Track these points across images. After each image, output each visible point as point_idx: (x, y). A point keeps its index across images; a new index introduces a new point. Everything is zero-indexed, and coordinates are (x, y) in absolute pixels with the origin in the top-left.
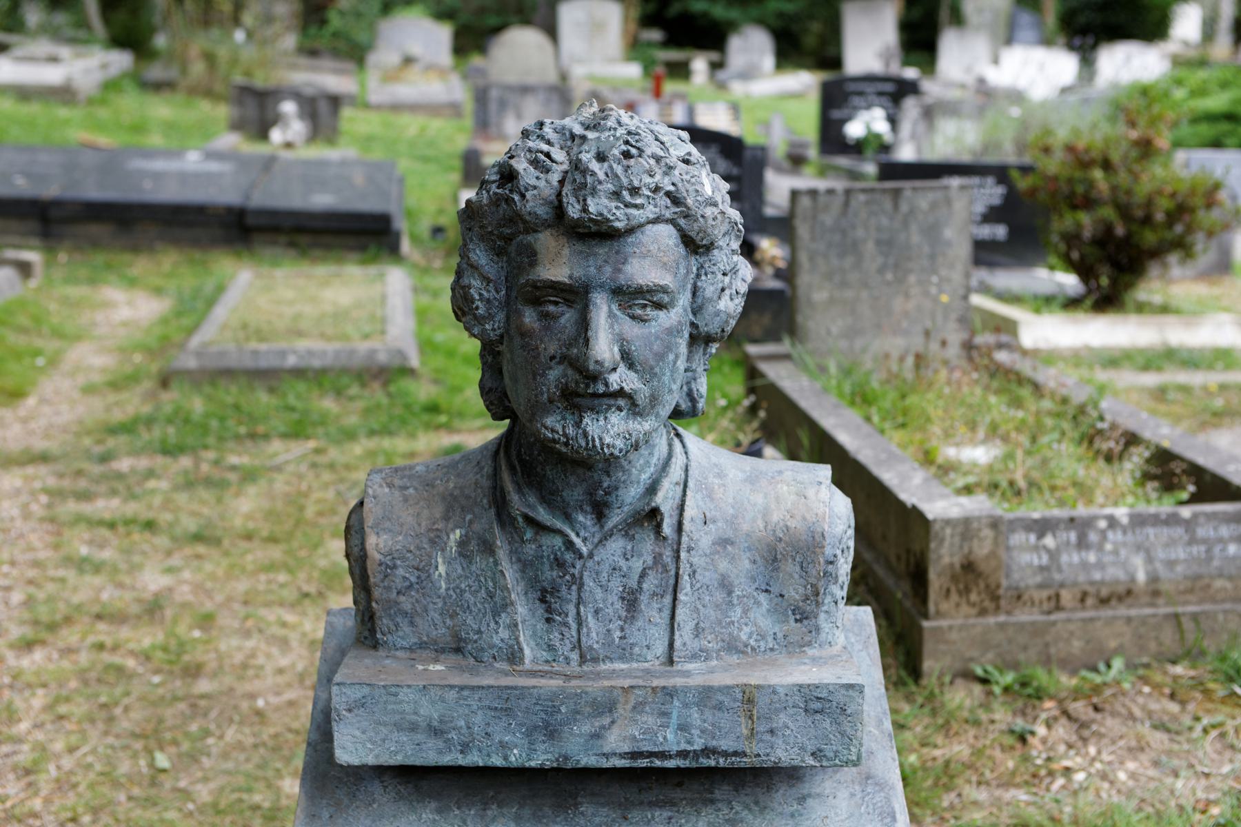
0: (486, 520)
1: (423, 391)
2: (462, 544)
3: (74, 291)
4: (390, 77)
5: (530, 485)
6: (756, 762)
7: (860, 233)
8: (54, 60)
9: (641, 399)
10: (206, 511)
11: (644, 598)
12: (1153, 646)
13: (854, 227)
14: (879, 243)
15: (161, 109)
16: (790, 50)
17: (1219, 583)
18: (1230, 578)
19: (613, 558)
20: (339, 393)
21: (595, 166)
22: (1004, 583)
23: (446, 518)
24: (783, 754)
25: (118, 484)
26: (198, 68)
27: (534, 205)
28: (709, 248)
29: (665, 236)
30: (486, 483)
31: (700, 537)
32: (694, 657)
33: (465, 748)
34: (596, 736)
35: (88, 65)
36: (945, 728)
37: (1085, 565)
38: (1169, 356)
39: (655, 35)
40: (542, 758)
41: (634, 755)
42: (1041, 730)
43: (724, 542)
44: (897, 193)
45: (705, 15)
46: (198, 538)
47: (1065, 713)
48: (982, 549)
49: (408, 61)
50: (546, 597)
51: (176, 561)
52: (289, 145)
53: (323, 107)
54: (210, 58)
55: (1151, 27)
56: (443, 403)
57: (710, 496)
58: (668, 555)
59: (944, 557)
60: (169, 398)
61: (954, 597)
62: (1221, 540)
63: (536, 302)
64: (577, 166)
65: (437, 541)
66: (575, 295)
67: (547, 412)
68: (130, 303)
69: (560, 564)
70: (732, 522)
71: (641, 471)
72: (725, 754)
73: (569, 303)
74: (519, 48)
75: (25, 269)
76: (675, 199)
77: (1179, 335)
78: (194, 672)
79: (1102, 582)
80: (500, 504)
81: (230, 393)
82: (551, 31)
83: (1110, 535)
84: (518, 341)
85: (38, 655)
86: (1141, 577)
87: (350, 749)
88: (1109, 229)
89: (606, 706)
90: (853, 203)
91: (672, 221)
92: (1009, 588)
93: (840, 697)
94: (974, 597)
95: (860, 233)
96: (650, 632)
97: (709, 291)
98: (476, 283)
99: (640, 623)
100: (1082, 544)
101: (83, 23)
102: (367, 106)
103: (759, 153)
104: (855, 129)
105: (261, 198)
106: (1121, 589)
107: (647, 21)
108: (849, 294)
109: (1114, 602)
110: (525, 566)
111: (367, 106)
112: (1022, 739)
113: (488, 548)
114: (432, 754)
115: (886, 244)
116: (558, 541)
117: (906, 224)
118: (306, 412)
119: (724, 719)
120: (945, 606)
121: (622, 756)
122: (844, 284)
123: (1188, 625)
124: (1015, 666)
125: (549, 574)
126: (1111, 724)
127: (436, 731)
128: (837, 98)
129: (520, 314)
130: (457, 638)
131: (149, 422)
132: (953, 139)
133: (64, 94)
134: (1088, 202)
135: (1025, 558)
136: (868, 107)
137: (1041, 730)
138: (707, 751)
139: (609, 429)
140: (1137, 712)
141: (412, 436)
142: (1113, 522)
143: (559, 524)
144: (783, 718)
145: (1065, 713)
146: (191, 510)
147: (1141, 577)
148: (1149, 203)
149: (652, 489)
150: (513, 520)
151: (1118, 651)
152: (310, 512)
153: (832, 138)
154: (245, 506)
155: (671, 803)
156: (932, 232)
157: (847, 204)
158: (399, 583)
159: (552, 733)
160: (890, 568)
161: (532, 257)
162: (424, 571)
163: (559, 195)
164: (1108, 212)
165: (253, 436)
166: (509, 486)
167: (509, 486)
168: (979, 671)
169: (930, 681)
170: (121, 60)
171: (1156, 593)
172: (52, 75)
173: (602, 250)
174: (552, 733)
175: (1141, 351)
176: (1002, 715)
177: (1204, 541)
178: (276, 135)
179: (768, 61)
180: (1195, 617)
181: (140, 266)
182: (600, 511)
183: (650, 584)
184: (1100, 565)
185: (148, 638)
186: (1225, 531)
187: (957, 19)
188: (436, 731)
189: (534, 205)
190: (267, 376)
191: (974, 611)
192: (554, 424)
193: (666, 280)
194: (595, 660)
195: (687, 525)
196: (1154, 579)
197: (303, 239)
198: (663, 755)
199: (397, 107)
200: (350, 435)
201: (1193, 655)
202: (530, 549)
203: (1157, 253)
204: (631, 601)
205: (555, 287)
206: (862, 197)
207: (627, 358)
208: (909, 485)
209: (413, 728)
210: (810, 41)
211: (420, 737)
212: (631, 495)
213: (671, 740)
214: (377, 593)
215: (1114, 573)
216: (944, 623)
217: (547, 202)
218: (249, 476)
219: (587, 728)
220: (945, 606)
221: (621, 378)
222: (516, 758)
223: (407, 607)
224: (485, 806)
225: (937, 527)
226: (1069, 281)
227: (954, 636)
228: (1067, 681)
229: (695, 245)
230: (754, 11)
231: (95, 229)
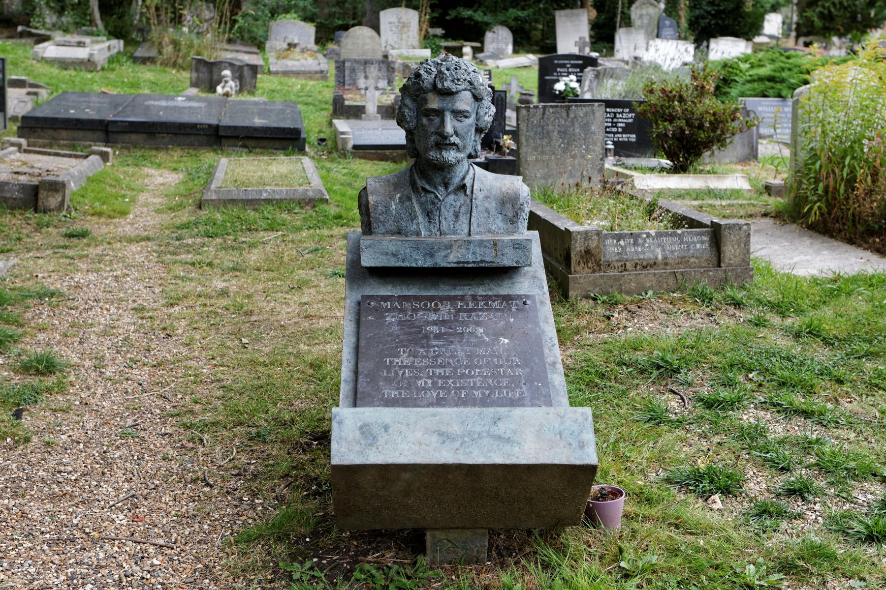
0: (408, 190)
1: (332, 210)
2: (400, 198)
3: (131, 170)
4: (282, 55)
5: (423, 178)
6: (498, 265)
7: (551, 127)
8: (80, 44)
9: (461, 146)
10: (235, 259)
11: (461, 215)
12: (665, 285)
13: (548, 124)
14: (559, 132)
15: (147, 74)
16: (522, 42)
17: (692, 260)
18: (697, 258)
19: (451, 202)
20: (289, 211)
21: (446, 72)
22: (603, 259)
23: (395, 190)
24: (507, 262)
25: (188, 249)
26: (169, 50)
27: (427, 84)
28: (482, 99)
29: (467, 95)
30: (408, 179)
31: (479, 195)
32: (477, 234)
33: (404, 260)
34: (446, 256)
35: (100, 48)
36: (578, 315)
37: (636, 252)
38: (710, 193)
39: (439, 31)
40: (428, 264)
41: (458, 263)
42: (616, 315)
43: (487, 197)
44: (569, 108)
45: (470, 18)
46: (234, 269)
47: (627, 309)
48: (593, 244)
49: (291, 46)
50: (429, 214)
51: (226, 277)
52: (227, 95)
53: (247, 72)
54: (176, 44)
55: (745, 26)
56: (344, 216)
57: (482, 182)
58: (468, 201)
59: (578, 247)
60: (204, 214)
61: (582, 265)
62: (693, 242)
63: (427, 115)
64: (440, 72)
65: (392, 198)
66: (440, 113)
67: (431, 151)
68: (161, 176)
69: (433, 203)
70: (489, 191)
71: (459, 172)
72: (488, 262)
73: (438, 116)
74: (358, 40)
75: (104, 156)
76: (471, 83)
77: (715, 183)
78: (251, 313)
79: (644, 259)
80: (413, 184)
81: (235, 211)
82: (376, 28)
83: (647, 240)
84: (421, 128)
85: (177, 308)
86: (660, 257)
87: (367, 261)
88: (682, 131)
89: (449, 247)
90: (547, 112)
91: (470, 90)
92: (605, 261)
93: (524, 243)
94: (590, 265)
95: (551, 127)
96: (463, 226)
97: (482, 113)
98: (407, 111)
99: (459, 223)
100: (636, 244)
101: (92, 22)
102: (270, 72)
103: (503, 95)
104: (559, 87)
105: (226, 121)
106: (652, 262)
107: (433, 23)
108: (546, 157)
109: (648, 268)
110: (421, 204)
111: (270, 72)
112: (609, 318)
113: (410, 199)
114: (393, 263)
115: (563, 133)
116: (433, 196)
117: (573, 124)
118: (274, 219)
119: (487, 251)
120: (578, 268)
121: (455, 263)
122: (543, 153)
123: (679, 277)
124: (607, 294)
125: (430, 207)
126: (644, 312)
127: (394, 255)
128: (548, 69)
129: (421, 120)
130: (399, 229)
131: (196, 224)
132: (611, 89)
133: (88, 64)
134: (671, 119)
135: (611, 250)
136: (569, 73)
137: (616, 315)
138: (482, 261)
139: (451, 156)
140: (655, 308)
141: (330, 229)
142: (648, 235)
143: (433, 190)
144: (506, 250)
145: (627, 309)
146: (228, 259)
147: (660, 257)
148: (701, 119)
149: (463, 178)
150: (417, 188)
151: (651, 287)
152: (286, 259)
153: (546, 91)
154: (254, 257)
155: (470, 285)
156: (586, 127)
157: (544, 114)
158: (379, 212)
159: (431, 255)
160: (558, 261)
161: (426, 101)
162: (387, 207)
163: (435, 81)
164: (682, 123)
165: (250, 230)
166: (416, 178)
167: (416, 178)
168: (592, 295)
169: (572, 299)
170: (118, 45)
171: (666, 264)
172: (81, 53)
173: (448, 99)
174: (431, 255)
175: (694, 190)
176: (601, 310)
177: (687, 243)
178: (219, 89)
179: (510, 48)
180: (682, 274)
181: (162, 156)
182: (446, 186)
183: (463, 210)
184: (643, 252)
185: (225, 302)
186: (695, 239)
187: (627, 22)
188: (394, 255)
189: (427, 84)
190: (252, 203)
191: (590, 271)
192: (433, 154)
193: (468, 108)
194: (445, 234)
195: (475, 191)
196: (665, 258)
197: (250, 143)
198: (468, 263)
199: (286, 73)
200: (299, 229)
201: (680, 288)
202: (423, 199)
203: (707, 144)
204: (457, 215)
205: (433, 110)
206: (551, 110)
207: (456, 133)
208: (563, 222)
209: (387, 254)
210: (536, 35)
211: (389, 257)
212: (456, 181)
213: (470, 258)
214: (372, 215)
215: (649, 255)
216: (578, 276)
217: (430, 84)
218: (252, 246)
219: (443, 254)
220: (578, 268)
221: (454, 139)
222: (420, 264)
223: (382, 220)
224: (408, 285)
225: (574, 235)
226: (666, 162)
227: (582, 281)
228: (629, 298)
229: (477, 98)
230: (501, 18)
231: (134, 137)
